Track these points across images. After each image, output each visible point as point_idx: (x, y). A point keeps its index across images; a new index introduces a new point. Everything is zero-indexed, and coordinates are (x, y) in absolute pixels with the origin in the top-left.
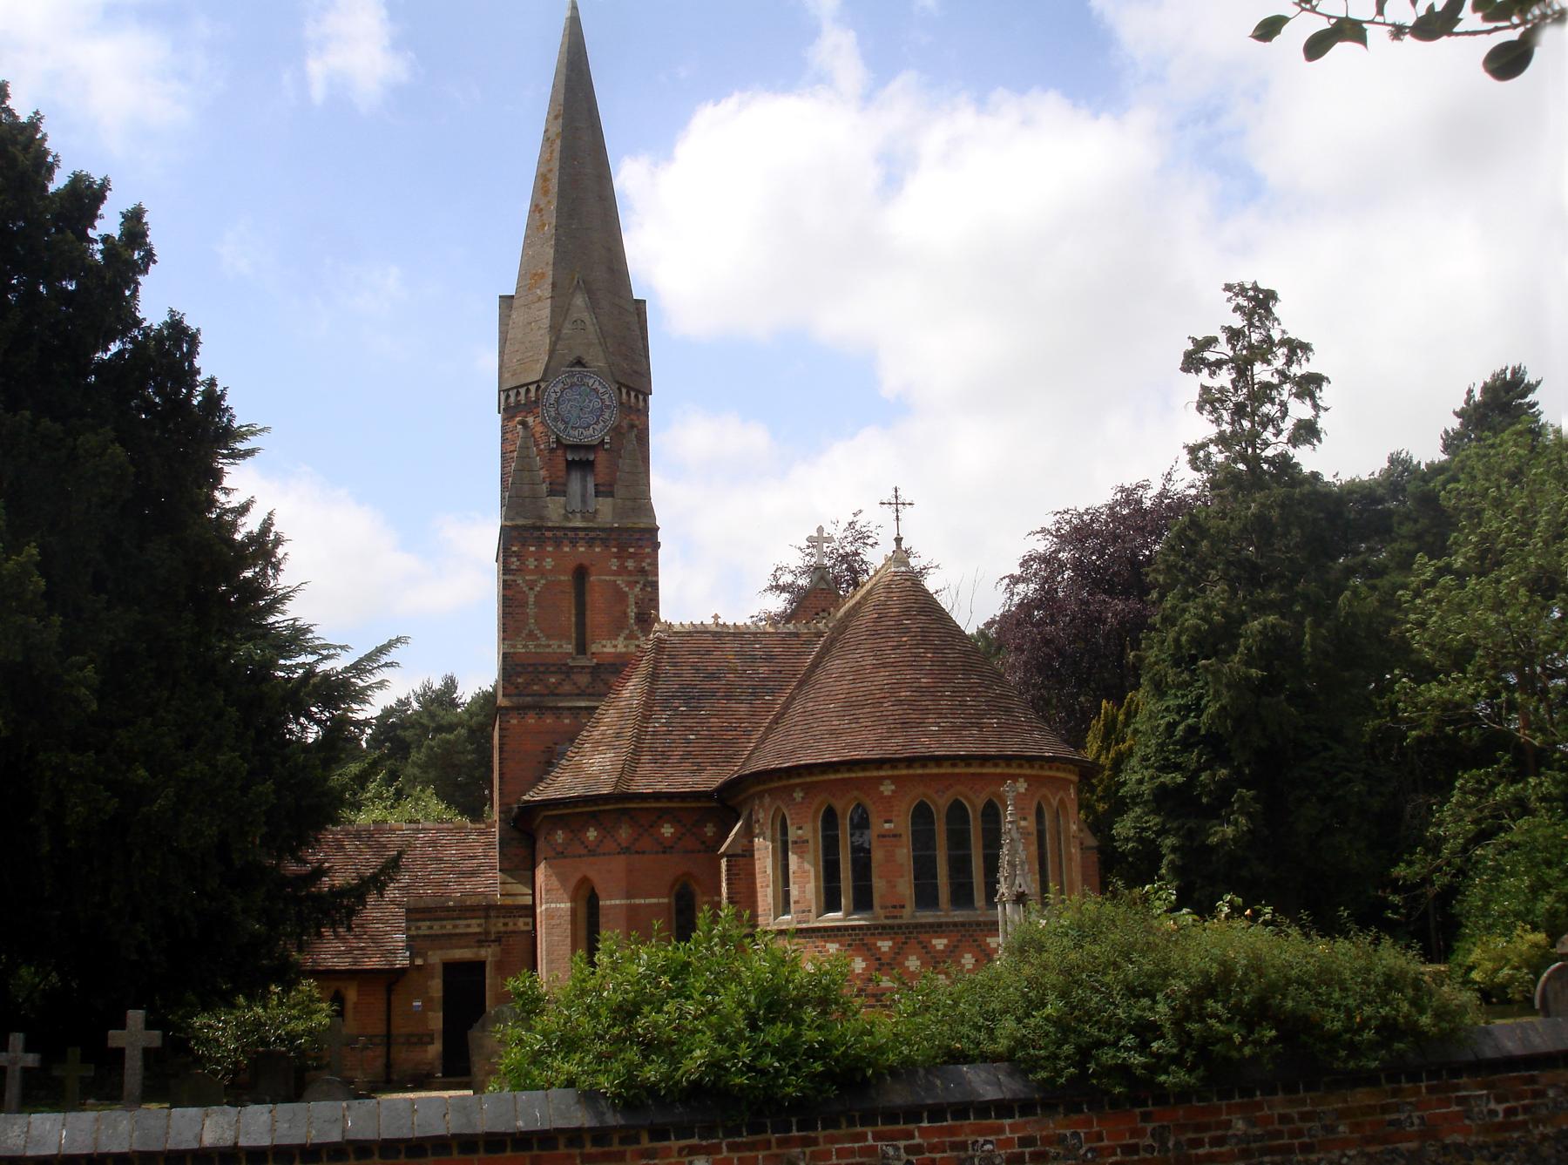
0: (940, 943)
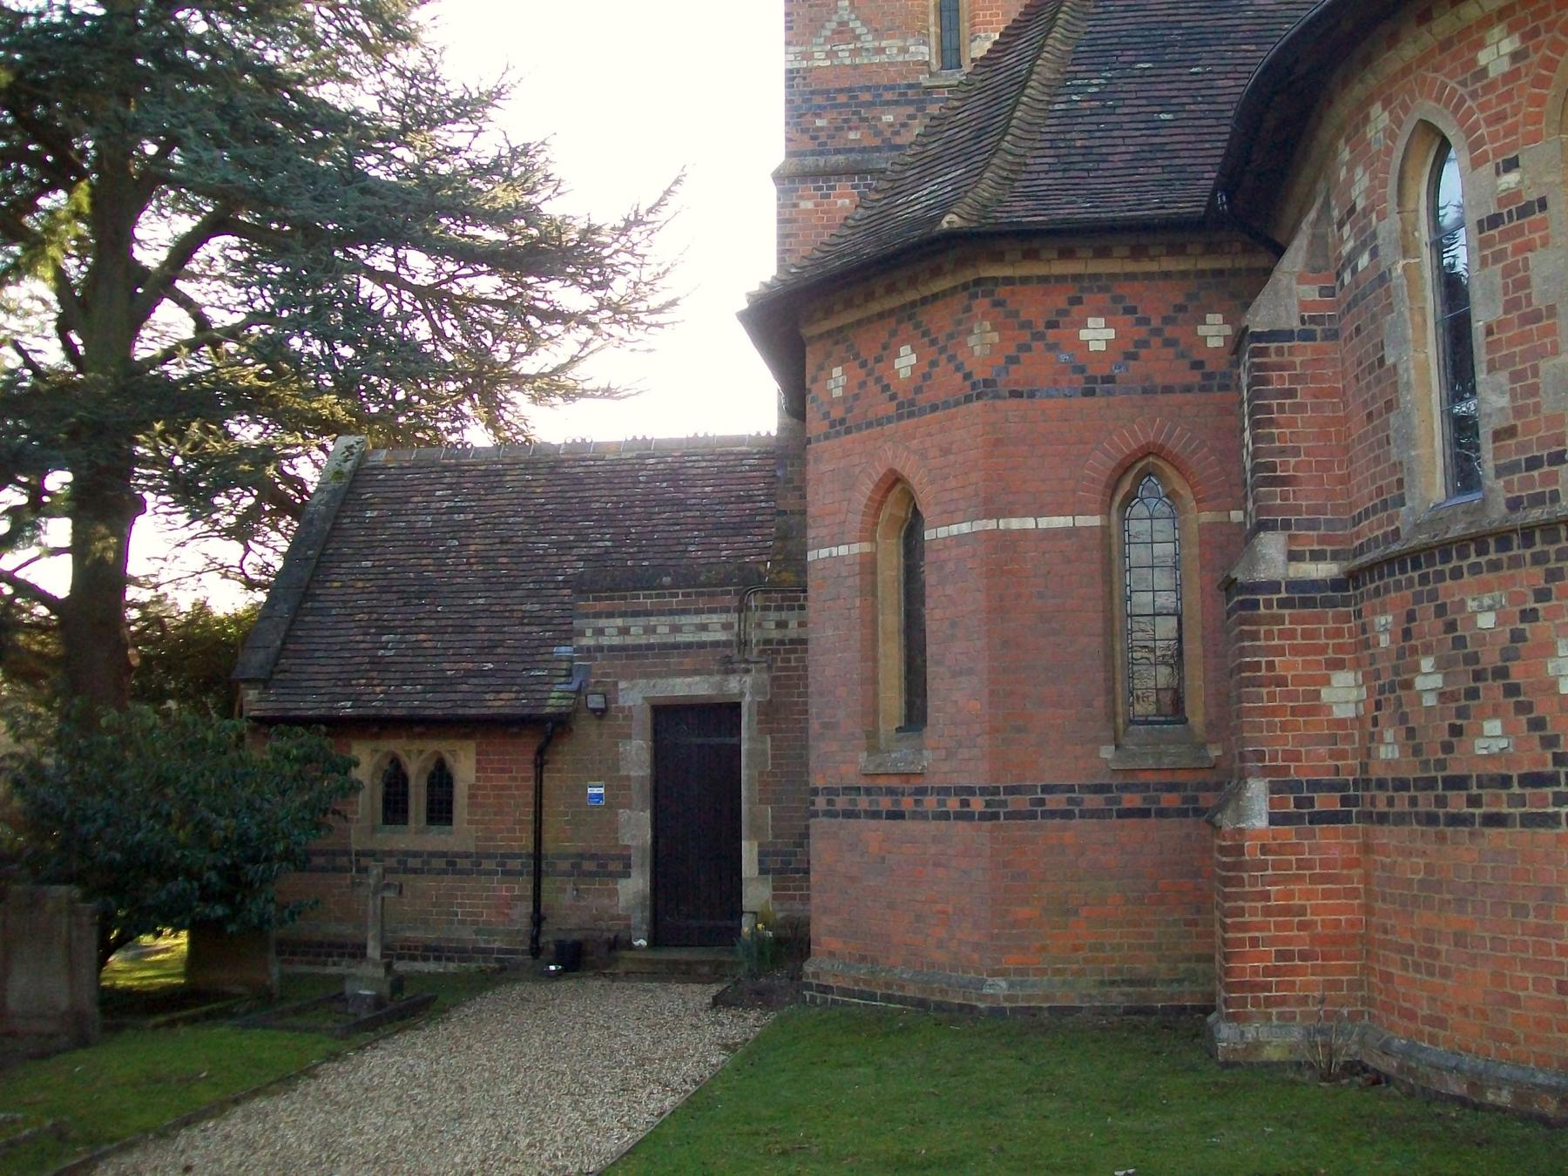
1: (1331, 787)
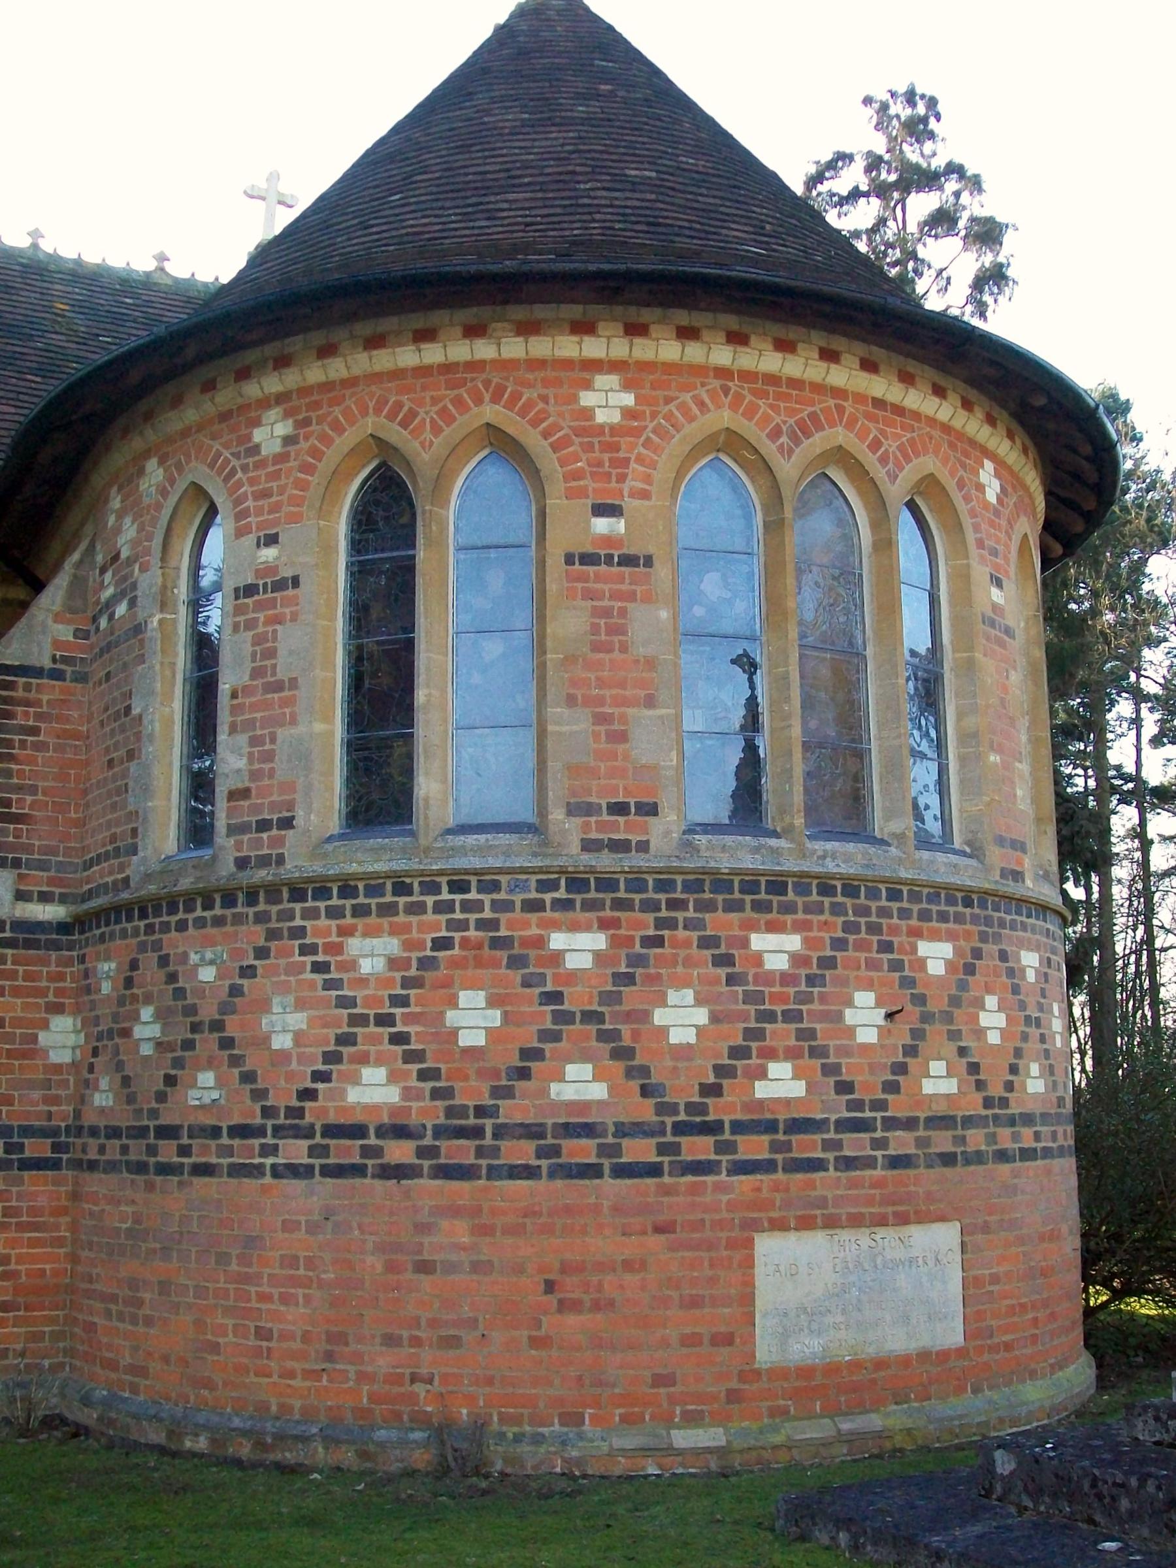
0: (776, 949)
1: (43, 1133)
